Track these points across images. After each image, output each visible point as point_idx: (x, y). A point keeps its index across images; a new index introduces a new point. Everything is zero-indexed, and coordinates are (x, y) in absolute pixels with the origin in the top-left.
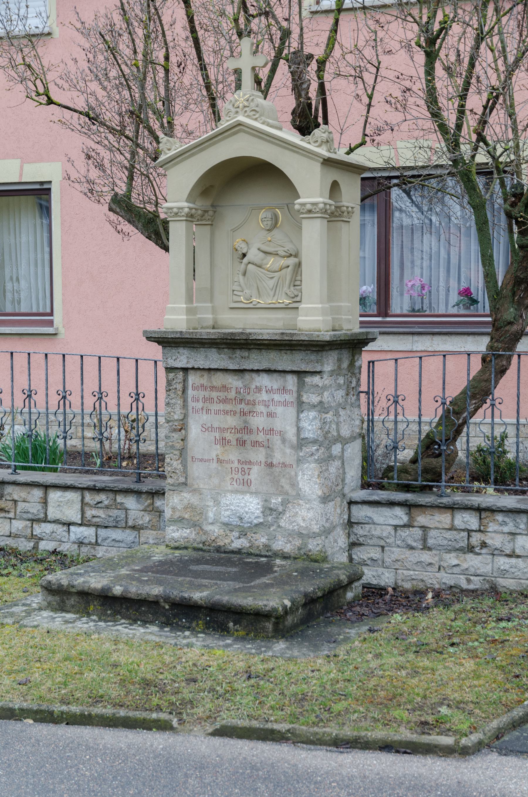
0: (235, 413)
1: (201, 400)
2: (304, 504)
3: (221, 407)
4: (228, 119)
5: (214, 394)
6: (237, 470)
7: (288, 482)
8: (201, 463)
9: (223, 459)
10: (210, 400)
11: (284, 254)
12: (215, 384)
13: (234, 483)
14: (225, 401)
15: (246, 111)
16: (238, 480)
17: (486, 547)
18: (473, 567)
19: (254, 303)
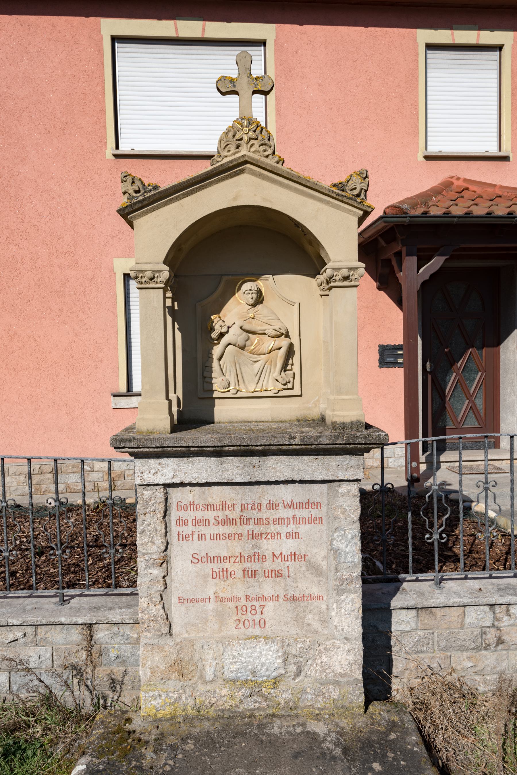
0: (240, 536)
1: (190, 523)
2: (342, 645)
3: (222, 529)
4: (226, 154)
5: (210, 515)
6: (244, 608)
7: (317, 618)
8: (192, 604)
9: (224, 596)
10: (205, 522)
11: (274, 333)
12: (210, 501)
13: (241, 625)
14: (226, 522)
15: (252, 145)
16: (246, 622)
17: (503, 643)
18: (489, 666)
19: (232, 392)
